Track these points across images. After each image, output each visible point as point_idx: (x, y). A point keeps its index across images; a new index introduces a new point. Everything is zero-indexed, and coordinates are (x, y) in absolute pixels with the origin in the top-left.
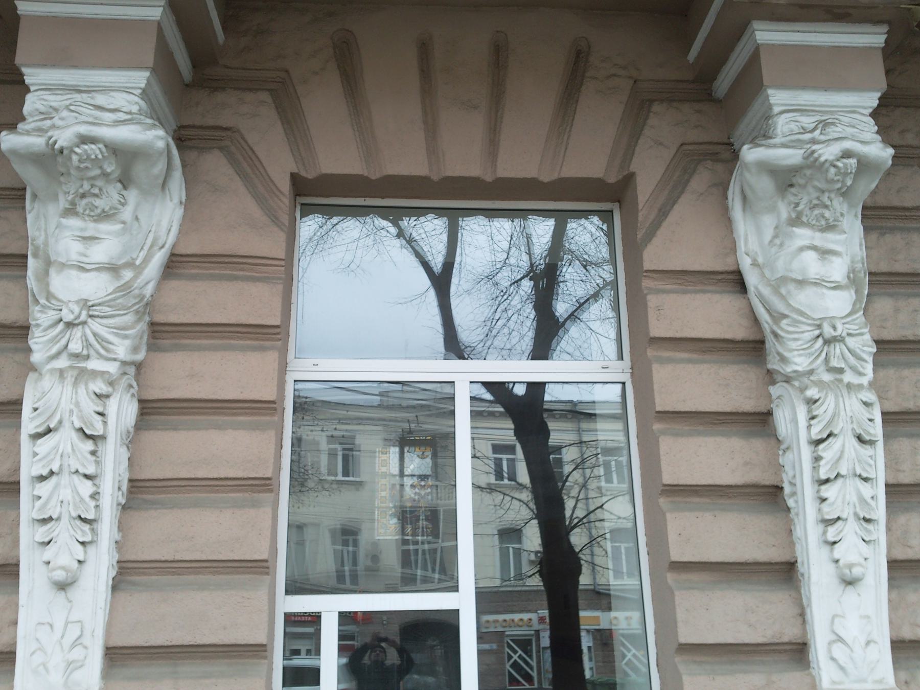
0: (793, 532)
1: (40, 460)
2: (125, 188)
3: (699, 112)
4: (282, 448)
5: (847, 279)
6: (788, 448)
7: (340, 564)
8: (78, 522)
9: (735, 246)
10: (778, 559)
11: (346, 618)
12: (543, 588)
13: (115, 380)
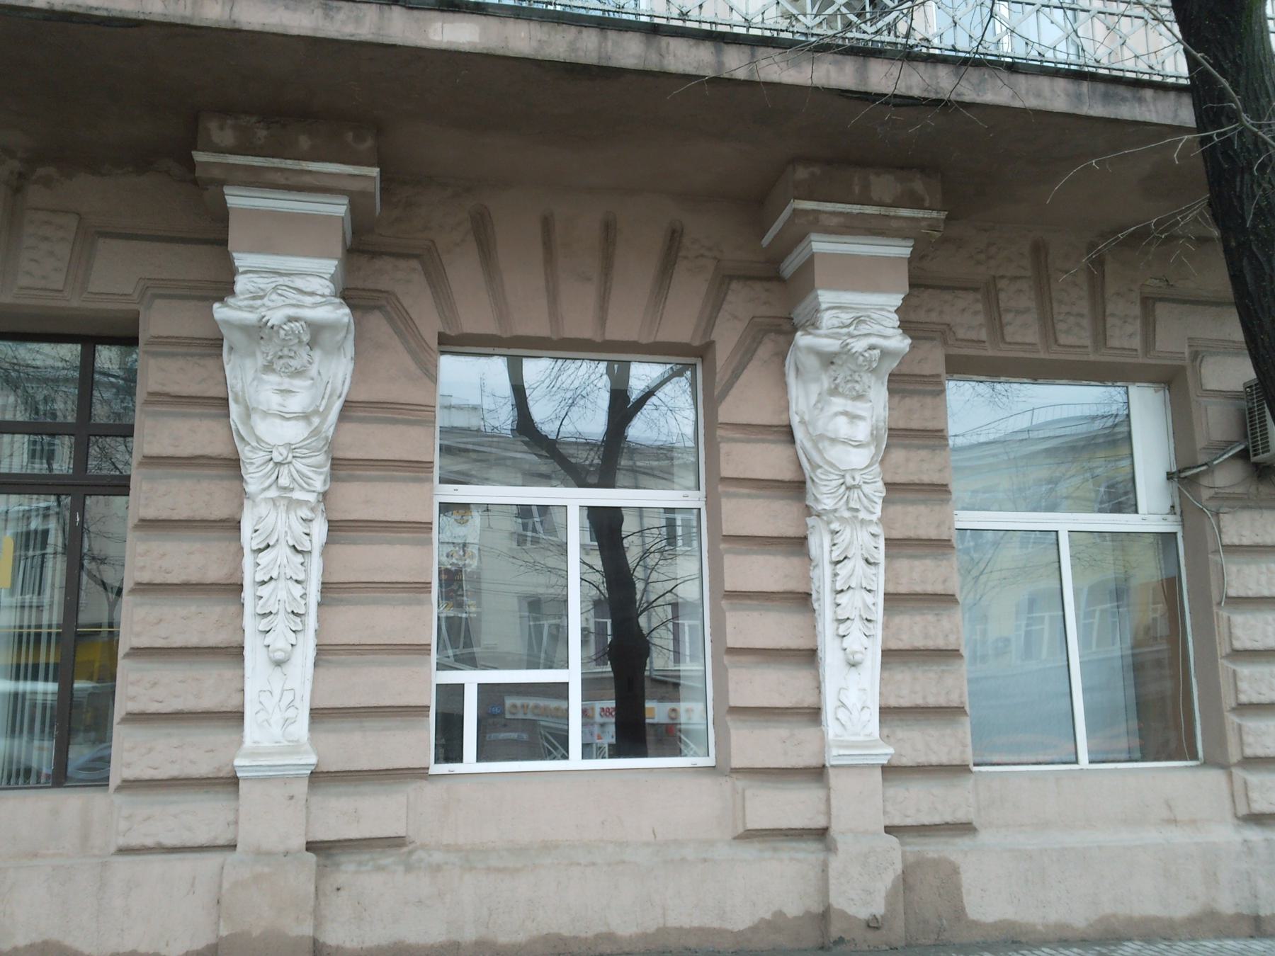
3: (767, 290)
8: (292, 616)
10: (805, 647)
11: (482, 688)
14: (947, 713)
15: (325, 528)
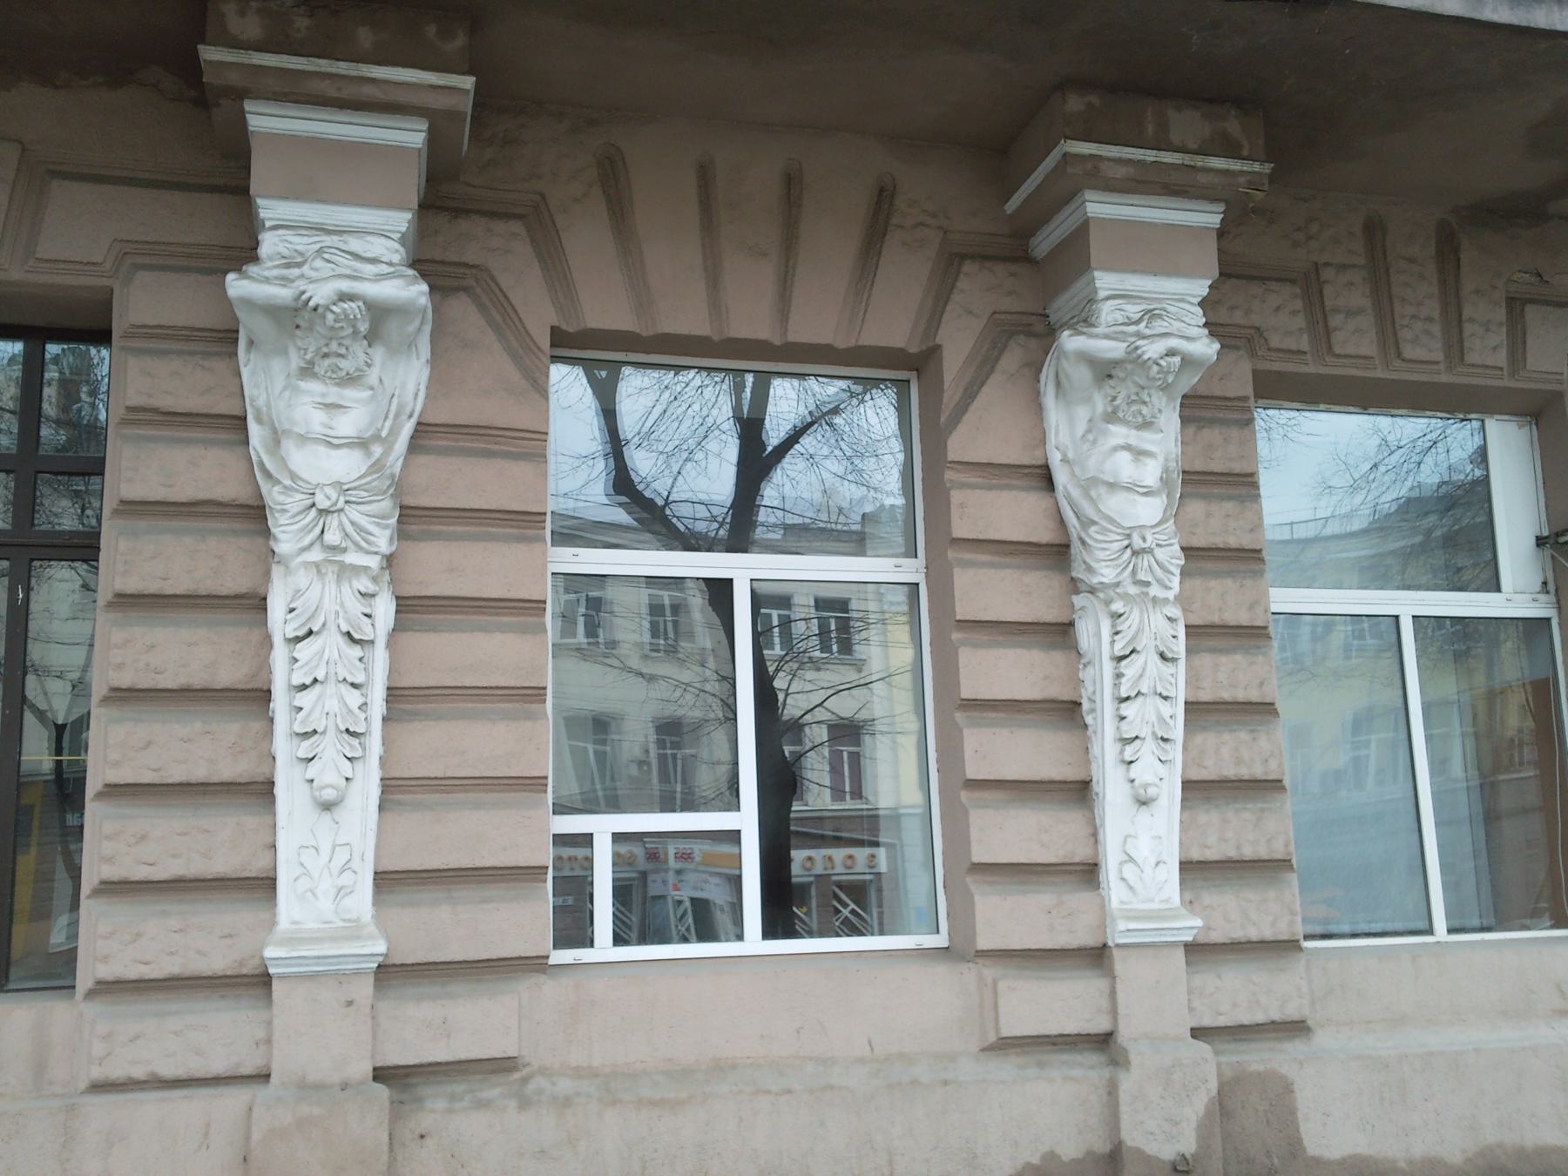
3: (1012, 275)
6: (1089, 663)
8: (346, 736)
14: (1268, 868)
15: (392, 607)
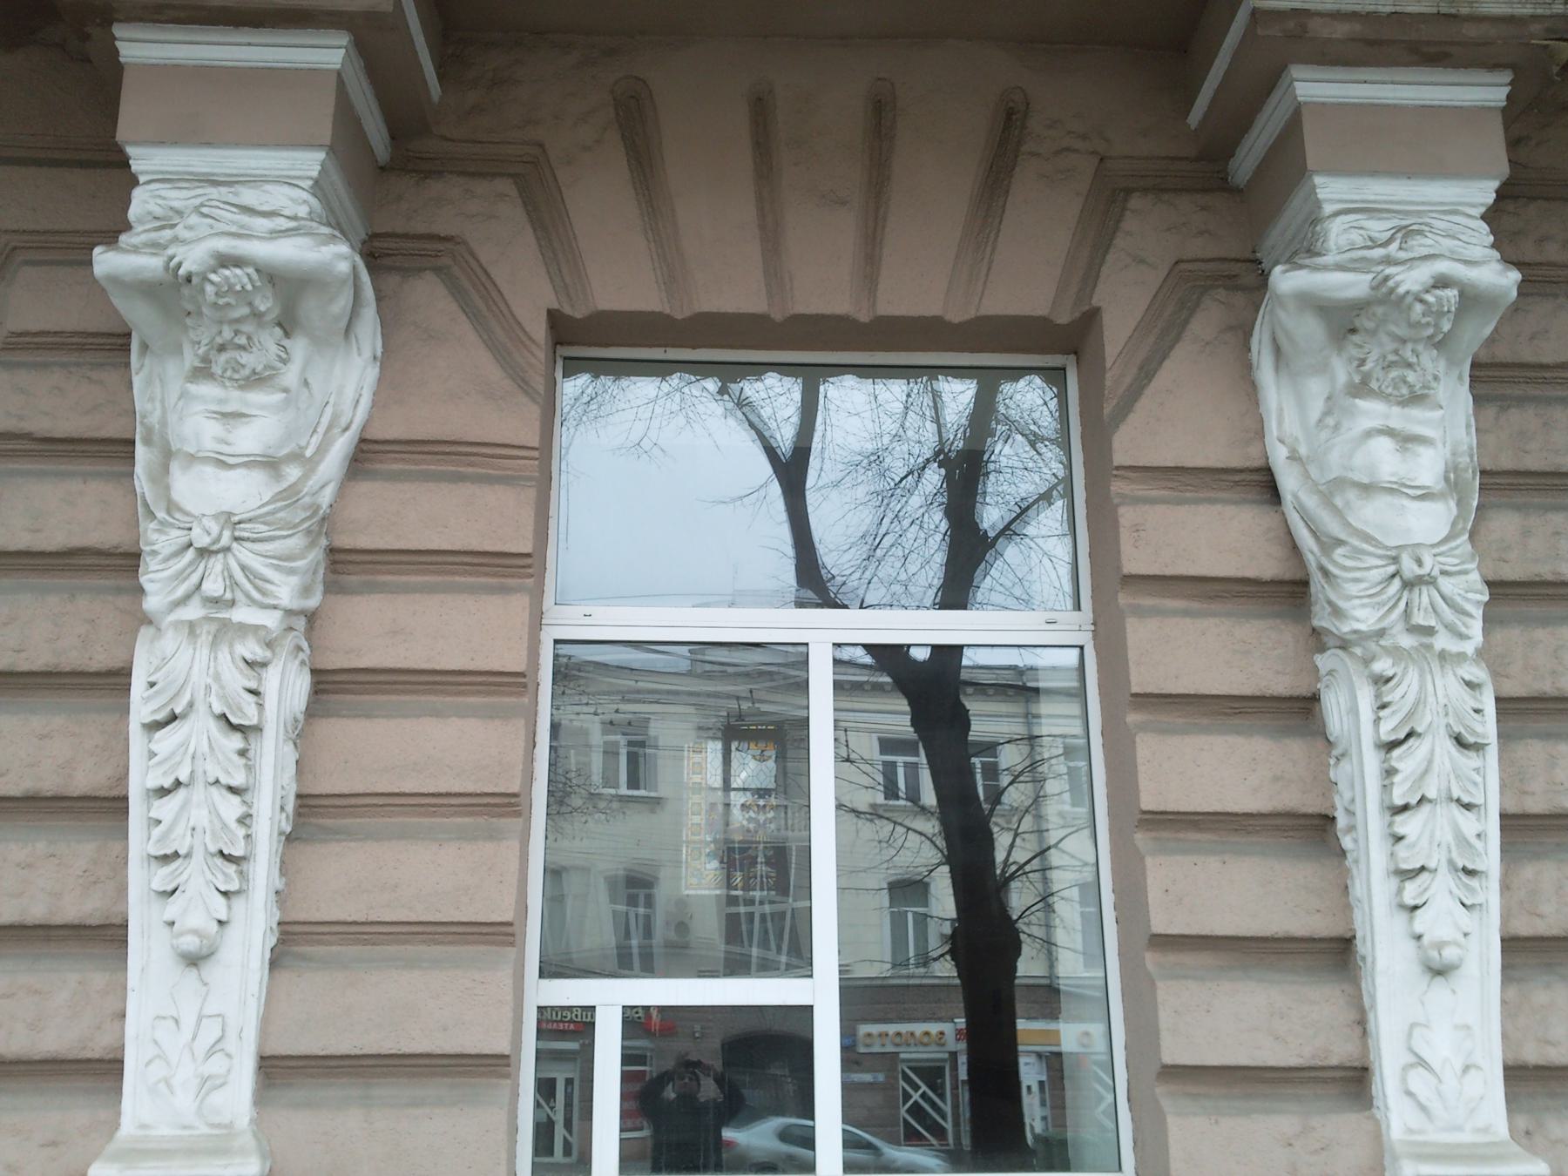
0: (1350, 890)
1: (160, 763)
2: (287, 335)
3: (1203, 208)
4: (534, 747)
5: (1443, 482)
6: (1343, 755)
7: (623, 935)
8: (219, 861)
9: (1263, 428)
10: (1325, 933)
11: (636, 1021)
12: (958, 981)
13: (276, 639)
